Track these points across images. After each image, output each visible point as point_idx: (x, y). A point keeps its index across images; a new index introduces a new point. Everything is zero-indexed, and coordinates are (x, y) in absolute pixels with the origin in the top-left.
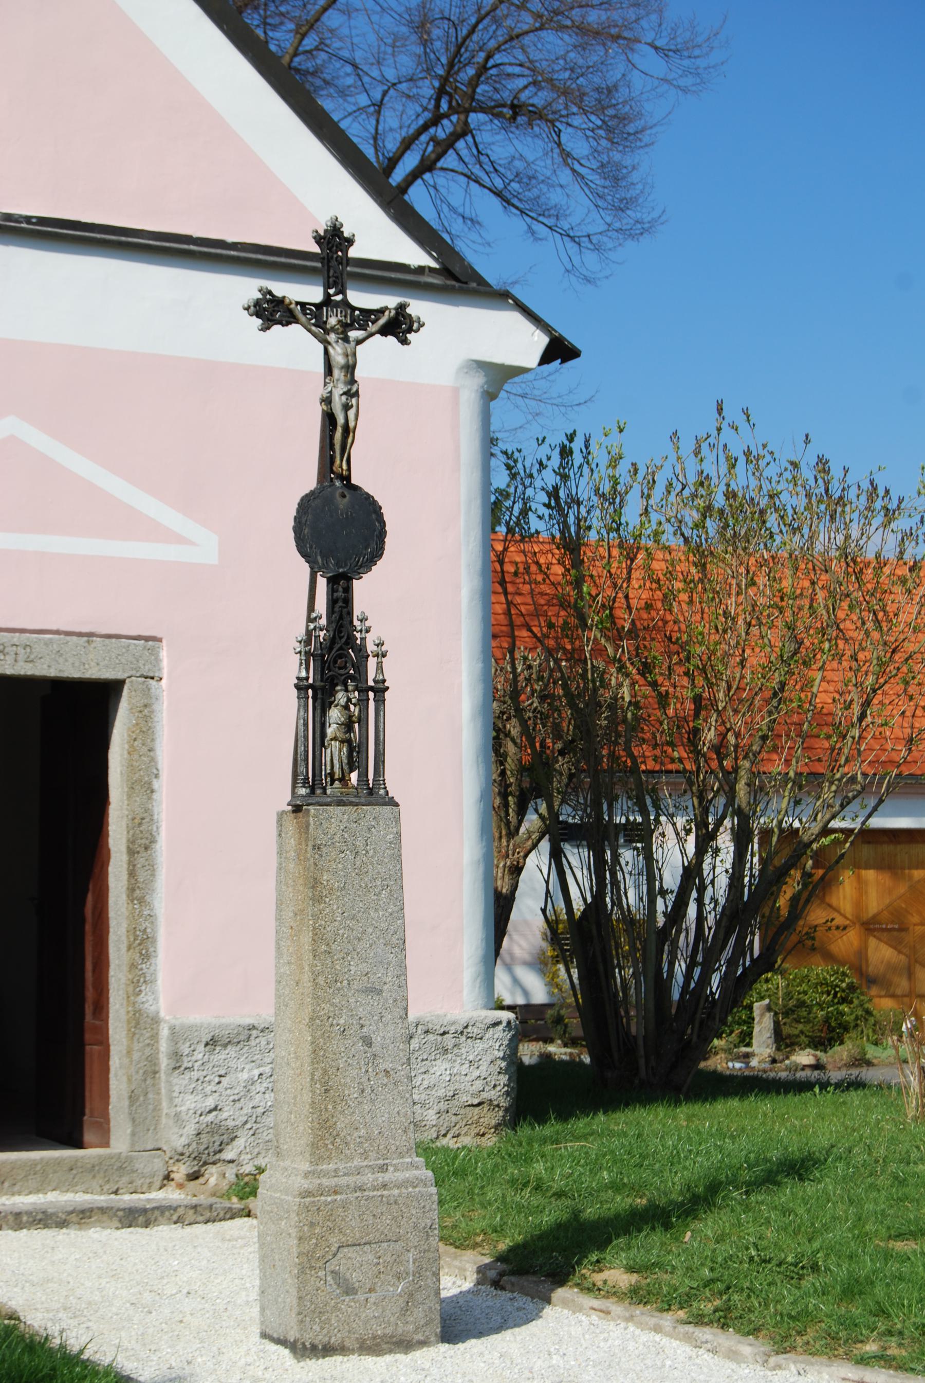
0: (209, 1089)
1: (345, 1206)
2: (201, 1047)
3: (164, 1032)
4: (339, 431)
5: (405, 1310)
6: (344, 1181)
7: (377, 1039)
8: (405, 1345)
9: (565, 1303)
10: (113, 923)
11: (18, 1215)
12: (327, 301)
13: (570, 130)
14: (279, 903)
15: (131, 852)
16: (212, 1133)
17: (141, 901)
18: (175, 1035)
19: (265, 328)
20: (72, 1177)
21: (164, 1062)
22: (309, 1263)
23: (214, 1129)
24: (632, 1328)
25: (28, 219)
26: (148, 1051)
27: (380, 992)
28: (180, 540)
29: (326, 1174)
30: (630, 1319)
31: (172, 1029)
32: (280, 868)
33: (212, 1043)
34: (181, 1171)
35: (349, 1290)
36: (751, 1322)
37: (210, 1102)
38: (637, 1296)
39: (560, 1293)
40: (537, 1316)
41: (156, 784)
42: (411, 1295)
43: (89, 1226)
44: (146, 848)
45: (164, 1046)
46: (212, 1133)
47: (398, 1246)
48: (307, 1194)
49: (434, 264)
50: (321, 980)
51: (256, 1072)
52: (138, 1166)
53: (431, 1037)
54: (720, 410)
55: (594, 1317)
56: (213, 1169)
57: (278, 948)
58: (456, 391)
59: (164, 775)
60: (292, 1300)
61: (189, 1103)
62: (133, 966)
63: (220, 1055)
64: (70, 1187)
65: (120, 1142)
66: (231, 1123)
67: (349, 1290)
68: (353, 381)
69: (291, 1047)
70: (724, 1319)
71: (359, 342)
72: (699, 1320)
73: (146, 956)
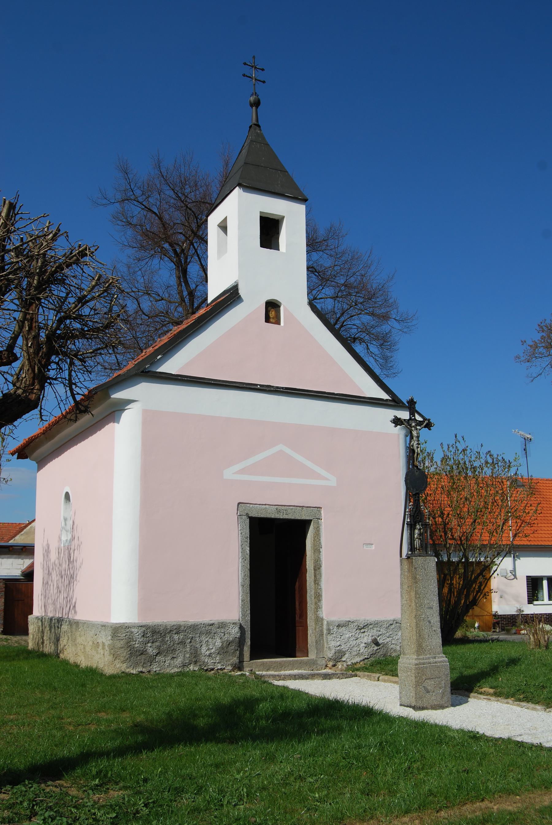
0: (338, 640)
1: (426, 668)
2: (336, 627)
3: (325, 623)
4: (416, 454)
5: (442, 697)
6: (425, 661)
7: (432, 621)
8: (442, 707)
9: (475, 697)
10: (308, 591)
11: (295, 675)
12: (410, 419)
13: (372, 345)
14: (402, 584)
15: (315, 570)
16: (339, 653)
17: (318, 584)
18: (328, 624)
19: (396, 427)
20: (301, 665)
21: (325, 632)
22: (418, 684)
23: (340, 651)
24: (499, 703)
25: (283, 388)
26: (320, 628)
27: (432, 608)
28: (327, 479)
29: (420, 659)
30: (498, 701)
31: (327, 622)
32: (401, 574)
33: (339, 626)
34: (330, 664)
35: (428, 692)
36: (535, 700)
37: (338, 644)
38: (497, 695)
39: (472, 694)
40: (467, 702)
41: (321, 550)
42: (443, 693)
43: (314, 679)
44: (319, 569)
45: (325, 627)
46: (339, 653)
47: (440, 679)
48: (416, 664)
49: (390, 399)
50: (418, 605)
51: (351, 635)
52: (319, 662)
53: (398, 624)
54: (456, 437)
55: (485, 701)
56: (339, 663)
57: (402, 596)
58: (399, 435)
59: (323, 547)
60: (413, 694)
61: (333, 644)
62: (316, 603)
63: (341, 630)
64: (300, 668)
65: (312, 655)
66: (344, 650)
67: (428, 692)
68: (419, 441)
69: (409, 624)
70: (527, 699)
71: (420, 430)
72: (520, 700)
73: (320, 601)
